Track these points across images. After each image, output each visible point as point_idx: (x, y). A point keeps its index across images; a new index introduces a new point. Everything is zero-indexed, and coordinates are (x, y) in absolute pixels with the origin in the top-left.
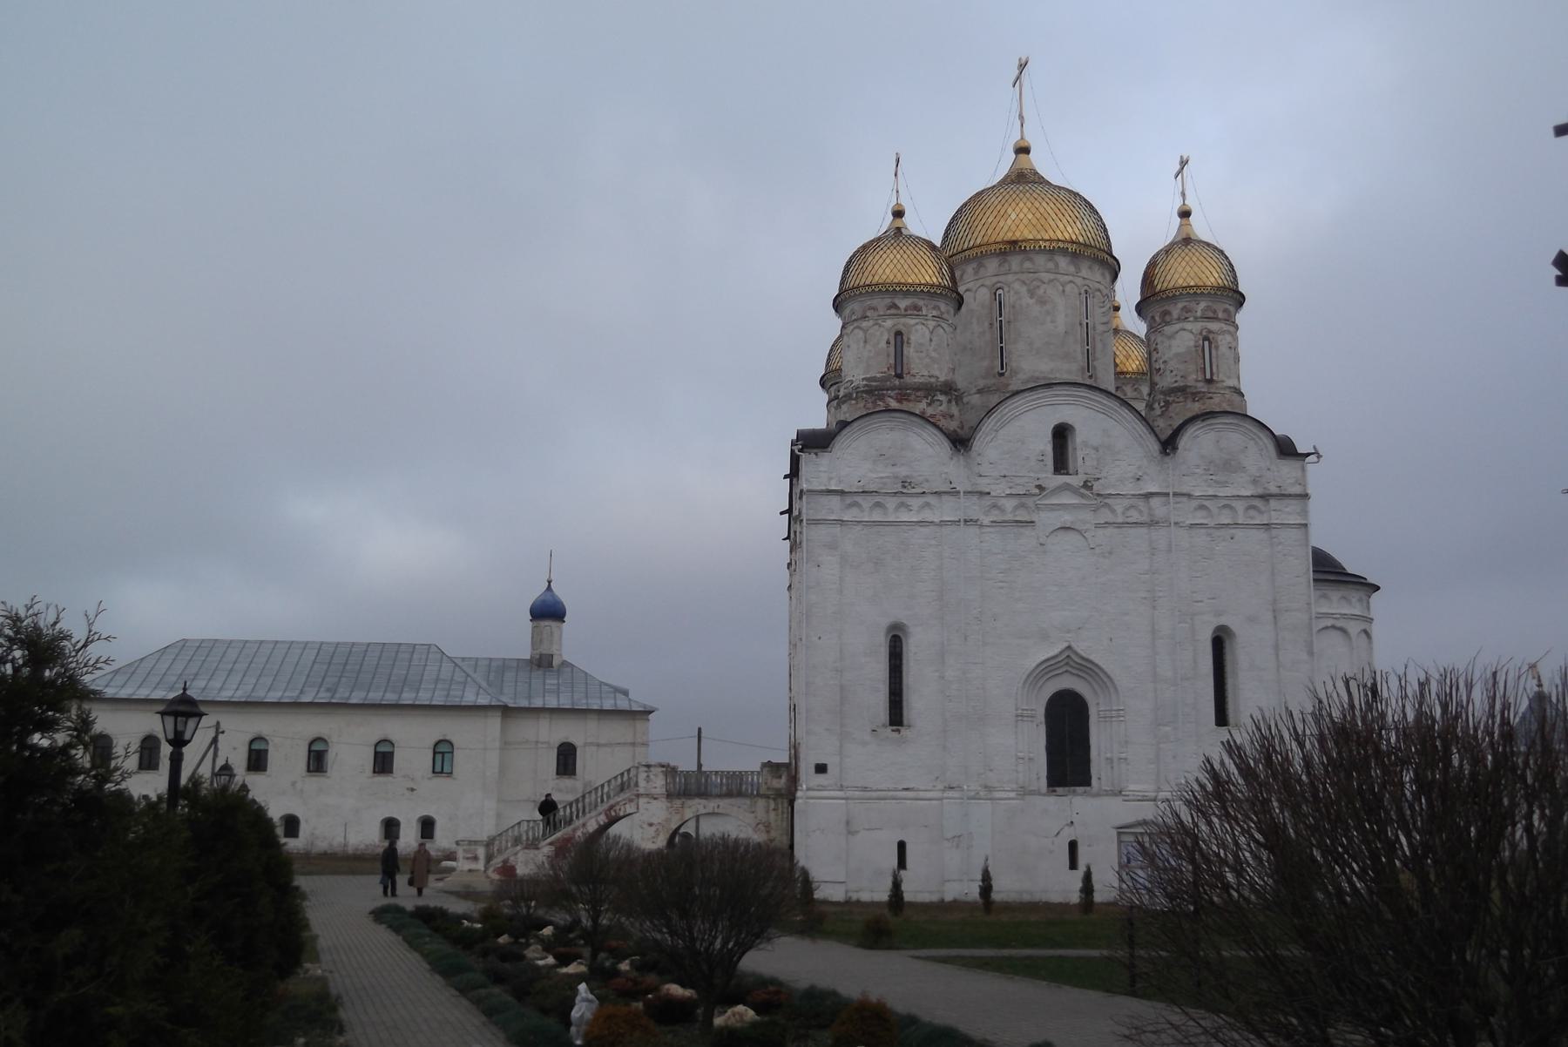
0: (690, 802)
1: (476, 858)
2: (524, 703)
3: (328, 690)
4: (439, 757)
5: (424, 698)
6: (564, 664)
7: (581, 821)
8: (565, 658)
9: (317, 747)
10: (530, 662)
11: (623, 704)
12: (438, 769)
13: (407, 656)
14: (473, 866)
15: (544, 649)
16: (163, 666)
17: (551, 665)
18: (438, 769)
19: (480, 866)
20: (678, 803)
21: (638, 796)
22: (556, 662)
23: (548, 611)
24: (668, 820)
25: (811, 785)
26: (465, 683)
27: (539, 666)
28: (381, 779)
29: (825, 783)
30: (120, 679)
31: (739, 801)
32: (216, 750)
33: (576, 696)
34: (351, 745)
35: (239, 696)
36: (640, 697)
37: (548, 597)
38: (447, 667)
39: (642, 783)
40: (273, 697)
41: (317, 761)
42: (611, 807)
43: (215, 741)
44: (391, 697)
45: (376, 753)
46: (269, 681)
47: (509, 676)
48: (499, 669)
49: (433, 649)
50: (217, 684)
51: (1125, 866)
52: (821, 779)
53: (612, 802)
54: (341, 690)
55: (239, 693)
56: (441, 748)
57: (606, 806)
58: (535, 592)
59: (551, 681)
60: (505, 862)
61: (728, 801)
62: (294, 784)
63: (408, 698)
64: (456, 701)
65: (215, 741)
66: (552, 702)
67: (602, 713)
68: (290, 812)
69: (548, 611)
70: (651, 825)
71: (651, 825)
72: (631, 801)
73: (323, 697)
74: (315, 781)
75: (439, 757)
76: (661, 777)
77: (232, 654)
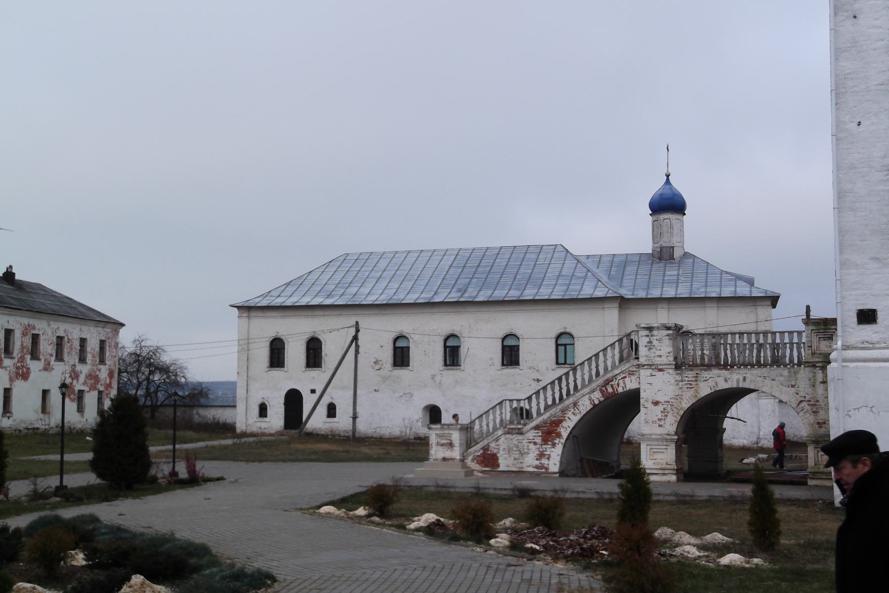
0: (705, 374)
1: (451, 445)
2: (641, 294)
3: (459, 290)
4: (561, 349)
5: (544, 293)
6: (686, 255)
7: (571, 400)
8: (688, 249)
9: (450, 343)
10: (652, 255)
11: (743, 290)
12: (561, 360)
13: (534, 256)
14: (448, 454)
15: (665, 242)
16: (326, 277)
17: (672, 257)
18: (561, 360)
19: (456, 453)
20: (690, 374)
21: (639, 366)
22: (677, 254)
23: (668, 205)
24: (678, 397)
25: (852, 340)
26: (585, 278)
27: (660, 259)
28: (510, 371)
29: (875, 338)
30: (290, 289)
31: (775, 371)
32: (357, 347)
33: (695, 285)
34: (481, 338)
35: (383, 299)
36: (764, 285)
37: (667, 191)
38: (570, 264)
39: (643, 351)
40: (411, 299)
41: (452, 355)
42: (607, 382)
43: (355, 338)
44: (514, 294)
45: (504, 347)
46: (408, 285)
47: (630, 270)
48: (620, 264)
49: (560, 248)
50: (365, 290)
51: (117, 531)
52: (867, 332)
53: (609, 376)
54: (470, 290)
55: (383, 297)
56: (562, 341)
57: (601, 381)
58: (653, 187)
59: (671, 272)
60: (486, 449)
61: (757, 371)
62: (433, 377)
63: (529, 294)
64: (573, 294)
65: (355, 338)
66: (670, 292)
67: (720, 300)
68: (432, 402)
69: (668, 205)
70: (656, 403)
71: (656, 403)
72: (631, 373)
73: (454, 297)
74: (451, 375)
75: (561, 349)
76: (667, 342)
77: (383, 264)
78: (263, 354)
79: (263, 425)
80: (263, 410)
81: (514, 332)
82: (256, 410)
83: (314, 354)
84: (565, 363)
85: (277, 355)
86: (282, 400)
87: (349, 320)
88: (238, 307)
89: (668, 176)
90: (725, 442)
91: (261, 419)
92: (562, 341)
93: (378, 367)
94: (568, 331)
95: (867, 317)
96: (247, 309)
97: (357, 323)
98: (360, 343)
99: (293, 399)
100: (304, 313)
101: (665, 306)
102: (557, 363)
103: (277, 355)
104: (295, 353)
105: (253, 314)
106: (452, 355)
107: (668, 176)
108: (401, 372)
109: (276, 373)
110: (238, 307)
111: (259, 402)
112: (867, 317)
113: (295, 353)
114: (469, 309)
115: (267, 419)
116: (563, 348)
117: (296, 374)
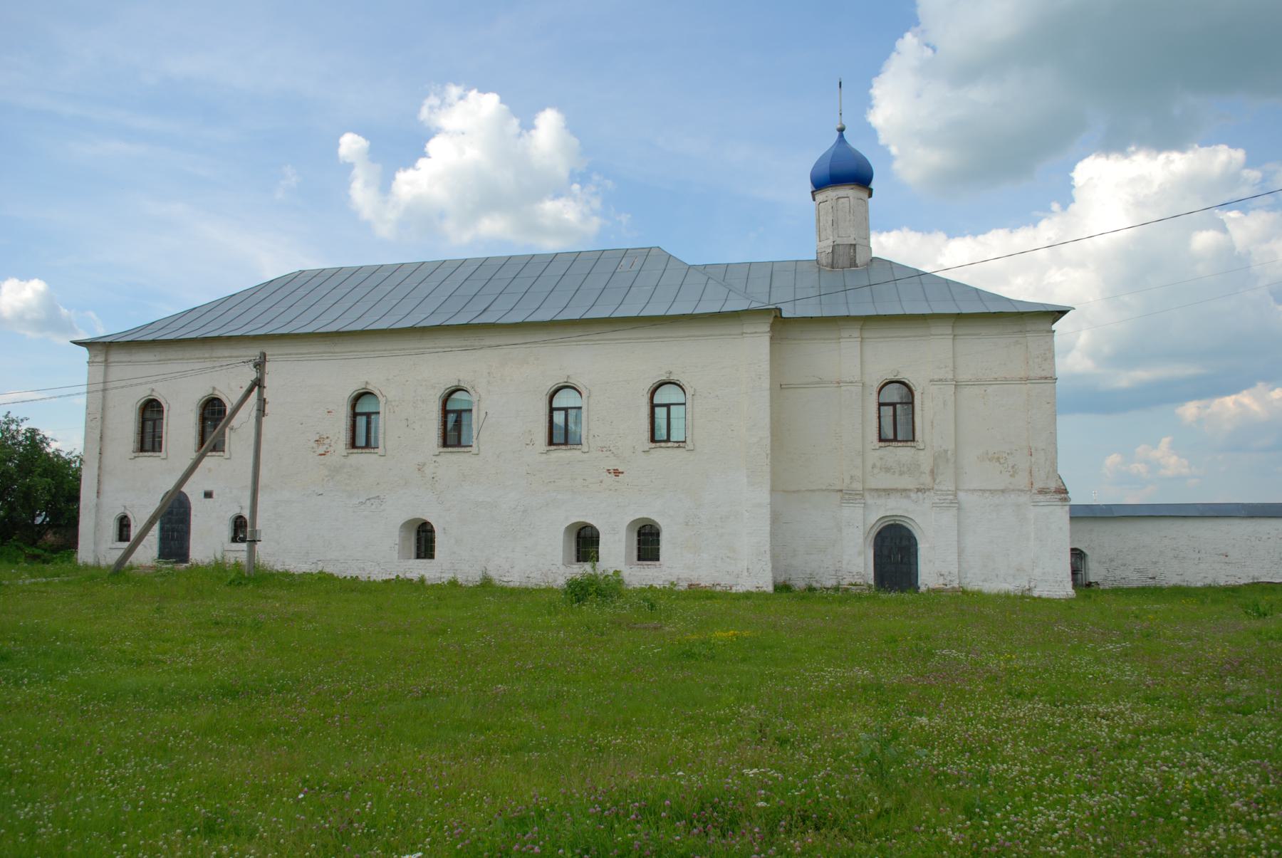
17: (853, 264)
32: (262, 402)
41: (453, 428)
43: (258, 383)
56: (663, 396)
62: (420, 468)
65: (258, 383)
74: (454, 458)
78: (126, 425)
81: (572, 382)
82: (112, 528)
84: (668, 440)
87: (254, 352)
89: (841, 130)
90: (80, 562)
92: (663, 396)
94: (674, 378)
95: (208, 495)
96: (101, 348)
98: (267, 394)
99: (174, 519)
100: (518, 338)
101: (856, 333)
102: (653, 440)
104: (181, 426)
105: (115, 356)
106: (453, 428)
107: (841, 130)
108: (361, 458)
109: (149, 461)
111: (118, 512)
112: (208, 495)
113: (181, 426)
114: (489, 340)
116: (665, 409)
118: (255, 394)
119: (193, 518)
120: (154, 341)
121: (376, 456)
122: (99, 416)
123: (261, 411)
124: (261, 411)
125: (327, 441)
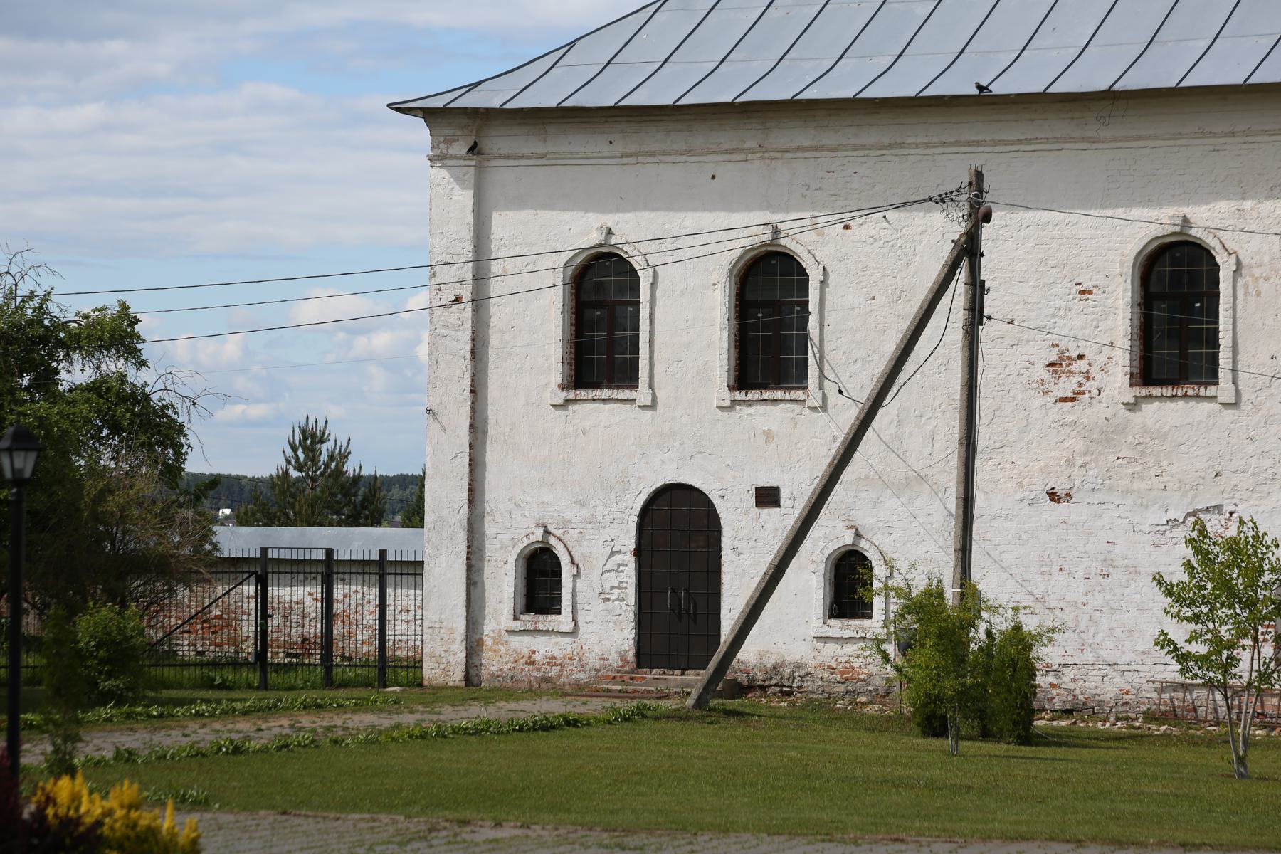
32: (977, 289)
43: (969, 250)
65: (969, 250)
78: (535, 325)
79: (543, 647)
80: (541, 580)
83: (770, 328)
85: (602, 331)
86: (627, 540)
88: (429, 115)
91: (529, 620)
93: (1066, 386)
96: (469, 130)
97: (979, 175)
99: (677, 531)
100: (726, 137)
103: (602, 331)
104: (688, 322)
105: (498, 141)
108: (1171, 413)
109: (602, 415)
110: (429, 115)
113: (688, 322)
115: (563, 621)
117: (687, 414)
118: (962, 275)
119: (724, 569)
120: (1111, 98)
121: (1206, 406)
122: (467, 294)
123: (976, 314)
124: (976, 314)
125: (1081, 366)
